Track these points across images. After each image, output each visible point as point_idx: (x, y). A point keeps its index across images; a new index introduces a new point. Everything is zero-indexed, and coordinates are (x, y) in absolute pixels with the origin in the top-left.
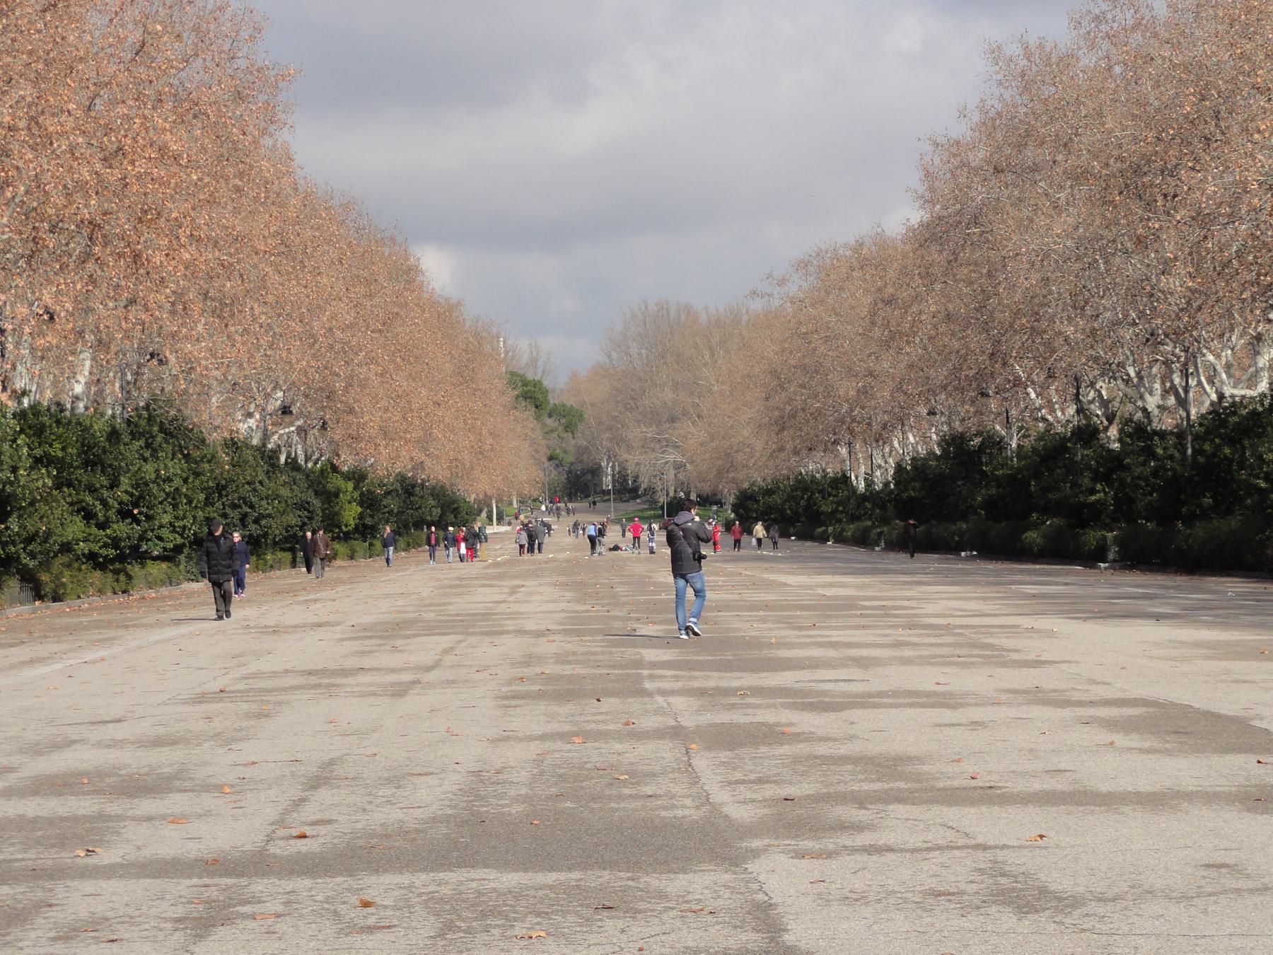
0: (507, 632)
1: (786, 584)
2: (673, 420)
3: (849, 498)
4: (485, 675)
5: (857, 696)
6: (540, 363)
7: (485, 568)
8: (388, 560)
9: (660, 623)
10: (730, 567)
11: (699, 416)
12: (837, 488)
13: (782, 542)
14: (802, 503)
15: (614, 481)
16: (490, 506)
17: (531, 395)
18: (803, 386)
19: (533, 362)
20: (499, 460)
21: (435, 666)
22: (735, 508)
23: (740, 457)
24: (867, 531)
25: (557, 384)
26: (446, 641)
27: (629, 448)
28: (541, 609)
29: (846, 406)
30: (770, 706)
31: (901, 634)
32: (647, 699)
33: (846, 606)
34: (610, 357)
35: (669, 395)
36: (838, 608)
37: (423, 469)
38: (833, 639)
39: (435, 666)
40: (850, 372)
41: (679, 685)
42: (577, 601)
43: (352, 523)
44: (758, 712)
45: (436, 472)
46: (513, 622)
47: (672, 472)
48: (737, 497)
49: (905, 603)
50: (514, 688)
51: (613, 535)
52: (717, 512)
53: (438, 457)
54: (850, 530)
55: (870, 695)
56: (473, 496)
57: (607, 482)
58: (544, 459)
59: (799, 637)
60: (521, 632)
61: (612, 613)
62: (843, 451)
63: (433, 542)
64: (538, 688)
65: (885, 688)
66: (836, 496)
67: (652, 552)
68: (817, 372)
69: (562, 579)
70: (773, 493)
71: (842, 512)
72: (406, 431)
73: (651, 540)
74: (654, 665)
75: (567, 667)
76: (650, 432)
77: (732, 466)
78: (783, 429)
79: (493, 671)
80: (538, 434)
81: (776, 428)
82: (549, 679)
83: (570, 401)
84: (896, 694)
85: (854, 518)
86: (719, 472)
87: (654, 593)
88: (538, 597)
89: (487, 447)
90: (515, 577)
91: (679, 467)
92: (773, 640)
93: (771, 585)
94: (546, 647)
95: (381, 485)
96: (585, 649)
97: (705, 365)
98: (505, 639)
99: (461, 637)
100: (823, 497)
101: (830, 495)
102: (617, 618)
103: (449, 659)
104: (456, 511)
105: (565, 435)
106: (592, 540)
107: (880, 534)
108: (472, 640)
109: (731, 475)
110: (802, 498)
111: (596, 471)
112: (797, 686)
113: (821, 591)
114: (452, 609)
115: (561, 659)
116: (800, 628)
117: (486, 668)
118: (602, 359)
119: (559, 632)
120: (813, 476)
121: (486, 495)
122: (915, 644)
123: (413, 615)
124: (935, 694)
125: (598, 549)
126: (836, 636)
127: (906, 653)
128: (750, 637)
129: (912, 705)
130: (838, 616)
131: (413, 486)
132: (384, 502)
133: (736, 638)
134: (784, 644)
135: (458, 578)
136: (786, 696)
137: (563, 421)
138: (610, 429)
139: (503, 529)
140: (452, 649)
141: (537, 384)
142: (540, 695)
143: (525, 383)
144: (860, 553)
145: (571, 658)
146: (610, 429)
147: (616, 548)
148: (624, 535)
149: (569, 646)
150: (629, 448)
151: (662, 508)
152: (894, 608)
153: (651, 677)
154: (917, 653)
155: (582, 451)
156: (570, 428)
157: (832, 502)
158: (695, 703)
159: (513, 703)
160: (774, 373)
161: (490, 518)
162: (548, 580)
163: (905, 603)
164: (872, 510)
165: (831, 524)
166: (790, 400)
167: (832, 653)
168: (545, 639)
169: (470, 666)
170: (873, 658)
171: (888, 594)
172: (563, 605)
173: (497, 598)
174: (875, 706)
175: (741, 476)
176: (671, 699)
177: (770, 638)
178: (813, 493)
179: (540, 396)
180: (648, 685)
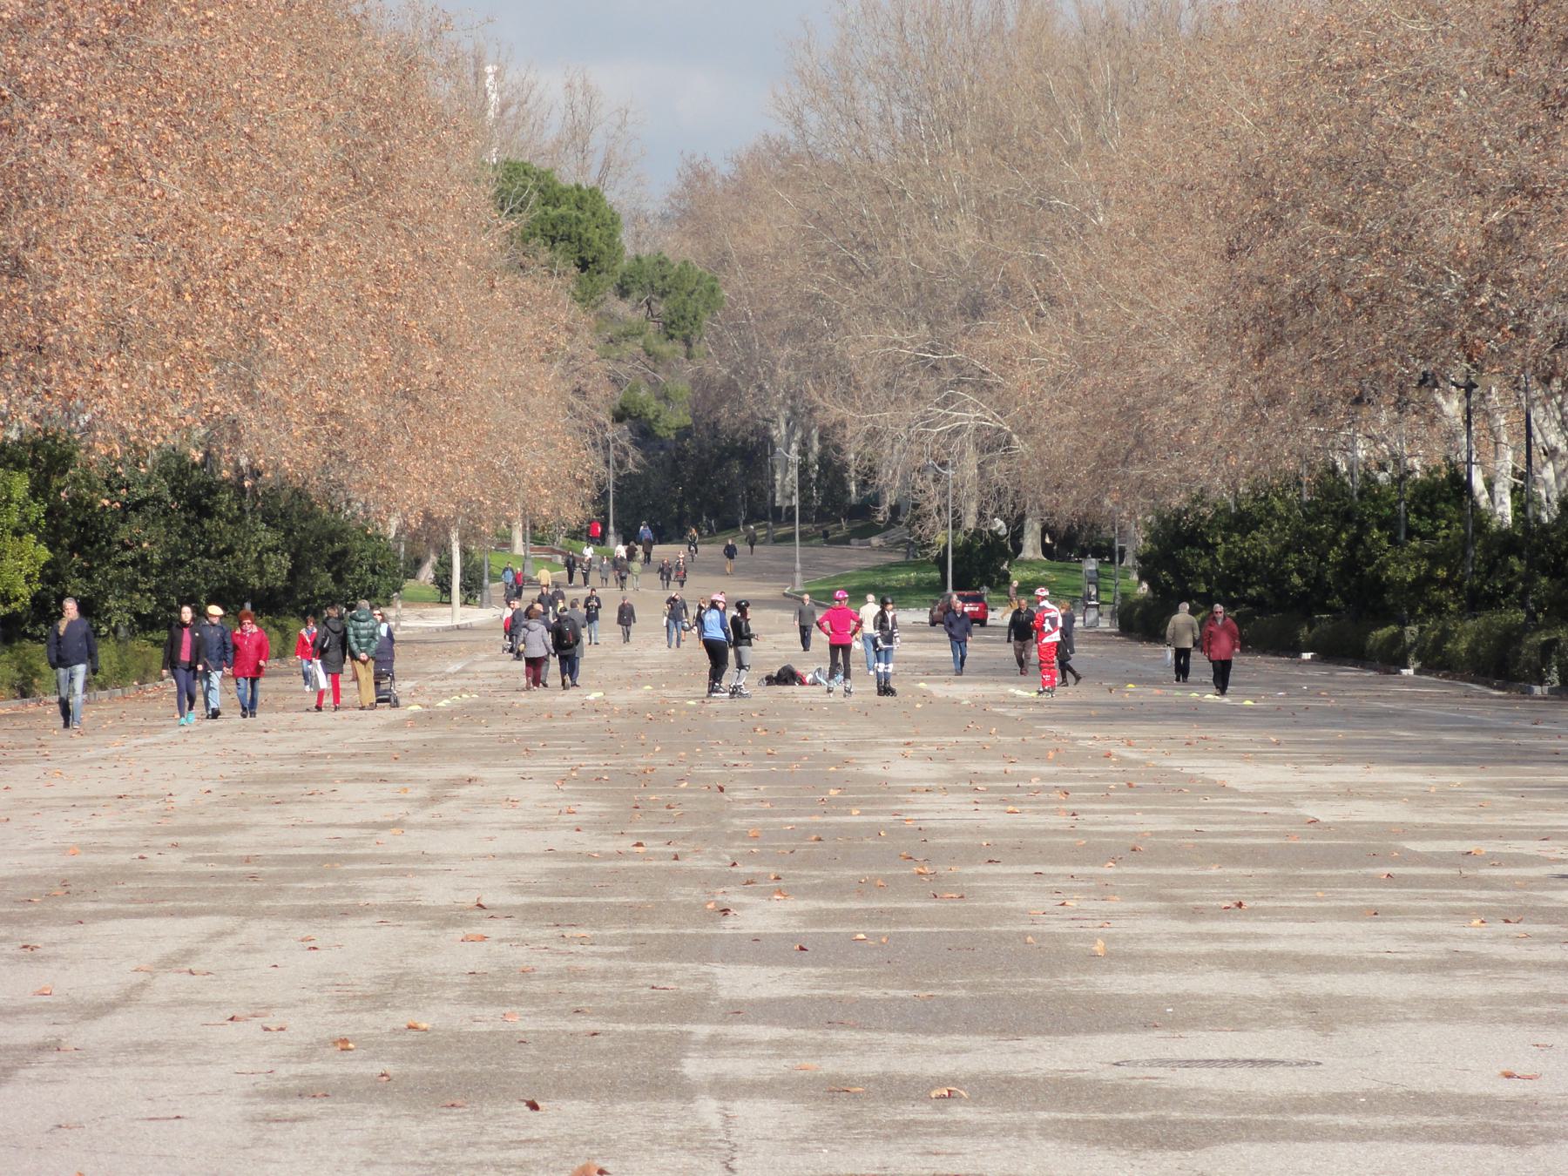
0: (366, 911)
1: (1222, 788)
2: (975, 309)
3: (1465, 542)
4: (252, 1028)
5: (1265, 1106)
6: (597, 140)
7: (390, 727)
8: (66, 710)
9: (812, 891)
10: (1087, 737)
11: (1051, 301)
12: (1434, 515)
13: (1243, 664)
14: (1333, 555)
15: (804, 486)
16: (444, 549)
17: (563, 228)
18: (1331, 218)
19: (578, 136)
20: (497, 416)
21: (127, 999)
22: (1149, 567)
23: (1160, 418)
24: (1511, 637)
25: (642, 202)
26: (175, 933)
27: (849, 386)
28: (492, 847)
29: (1458, 278)
30: (1006, 1131)
31: (1475, 937)
32: (672, 1106)
33: (1363, 852)
34: (798, 124)
35: (966, 237)
36: (1334, 857)
37: (236, 440)
38: (1273, 946)
39: (127, 999)
40: (1469, 183)
41: (782, 1066)
42: (601, 825)
43: (23, 591)
44: (967, 1144)
45: (276, 446)
46: (392, 883)
47: (971, 460)
48: (1154, 538)
49: (1531, 847)
50: (316, 1067)
51: (775, 638)
52: (1096, 579)
53: (280, 407)
54: (1466, 634)
55: (1302, 1104)
56: (394, 523)
57: (785, 485)
58: (604, 417)
59: (1184, 937)
60: (405, 911)
61: (686, 863)
62: (1452, 407)
63: (185, 656)
64: (377, 1068)
65: (1354, 1084)
66: (1430, 536)
67: (885, 690)
68: (1375, 179)
69: (590, 763)
70: (1255, 525)
71: (1445, 584)
72: (182, 328)
73: (882, 655)
74: (737, 1011)
75: (490, 1012)
76: (910, 341)
77: (1139, 443)
78: (1278, 339)
79: (273, 1021)
80: (585, 345)
81: (1251, 338)
82: (420, 1041)
83: (678, 248)
84: (1377, 1102)
85: (1477, 602)
86: (1104, 461)
87: (829, 806)
88: (502, 814)
89: (422, 381)
90: (462, 755)
91: (992, 444)
92: (1099, 947)
93: (1173, 788)
94: (455, 955)
95: (112, 483)
96: (563, 963)
97: (1073, 152)
98: (353, 932)
99: (229, 922)
100: (1393, 540)
101: (1411, 532)
102: (693, 876)
103: (169, 983)
104: (339, 564)
105: (665, 348)
106: (716, 652)
107: (1548, 648)
108: (257, 930)
109: (1136, 471)
110: (1334, 541)
111: (753, 454)
112: (1110, 1075)
113: (1311, 810)
114: (238, 843)
115: (483, 988)
116: (1195, 914)
117: (259, 1010)
118: (781, 130)
119: (508, 913)
120: (1368, 479)
121: (428, 516)
122: (1505, 965)
123: (124, 858)
124: (1490, 1103)
125: (730, 676)
126: (1288, 936)
127: (1466, 987)
128: (1043, 936)
129: (1404, 1134)
130: (1322, 882)
131: (212, 490)
132: (123, 533)
133: (1001, 937)
134: (1129, 957)
135: (305, 757)
136: (1067, 1104)
137: (661, 308)
138: (796, 333)
139: (458, 614)
140: (189, 954)
141: (587, 199)
142: (381, 1089)
143: (551, 195)
144: (1485, 704)
145: (513, 987)
146: (796, 333)
147: (787, 677)
148: (805, 641)
149: (520, 955)
150: (849, 386)
151: (941, 562)
152: (1495, 860)
153: (714, 1045)
154: (1493, 990)
155: (710, 394)
156: (677, 327)
157: (1419, 554)
158: (800, 1117)
159: (294, 1108)
160: (1254, 178)
161: (443, 584)
162: (555, 765)
163: (1531, 847)
164: (1529, 579)
165: (1413, 617)
166: (1295, 259)
167: (1254, 985)
168: (459, 933)
169: (218, 1005)
170: (1366, 1001)
171: (1498, 820)
172: (558, 839)
173: (379, 814)
174: (1306, 1134)
175: (1163, 474)
176: (739, 1107)
177: (1092, 939)
178: (1363, 527)
179: (594, 234)
180: (693, 1067)
